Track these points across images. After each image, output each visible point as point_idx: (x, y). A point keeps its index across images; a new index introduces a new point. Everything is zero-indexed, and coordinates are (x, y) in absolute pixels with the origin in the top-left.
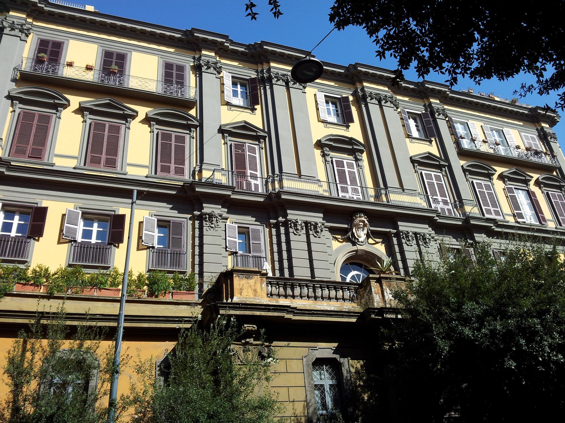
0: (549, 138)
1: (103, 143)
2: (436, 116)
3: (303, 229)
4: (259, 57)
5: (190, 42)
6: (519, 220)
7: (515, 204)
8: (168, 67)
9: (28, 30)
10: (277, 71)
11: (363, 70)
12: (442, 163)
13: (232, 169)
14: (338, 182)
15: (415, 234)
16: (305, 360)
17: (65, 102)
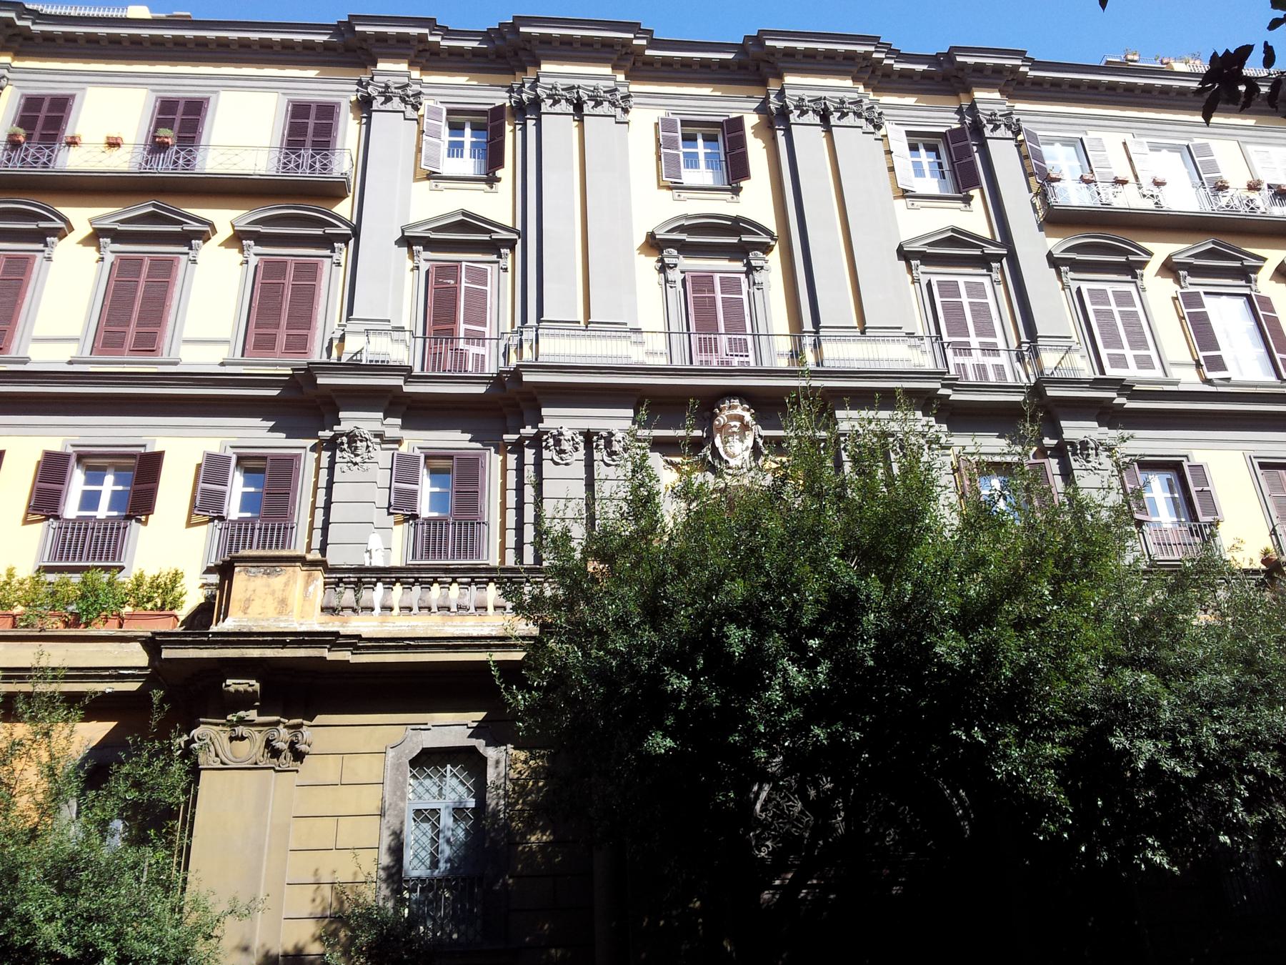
1: (135, 306)
3: (577, 449)
4: (516, 54)
5: (350, 48)
6: (1210, 375)
7: (1202, 332)
9: (418, 94)
10: (593, 83)
11: (780, 44)
13: (688, 329)
14: (693, 329)
16: (391, 753)
17: (59, 224)
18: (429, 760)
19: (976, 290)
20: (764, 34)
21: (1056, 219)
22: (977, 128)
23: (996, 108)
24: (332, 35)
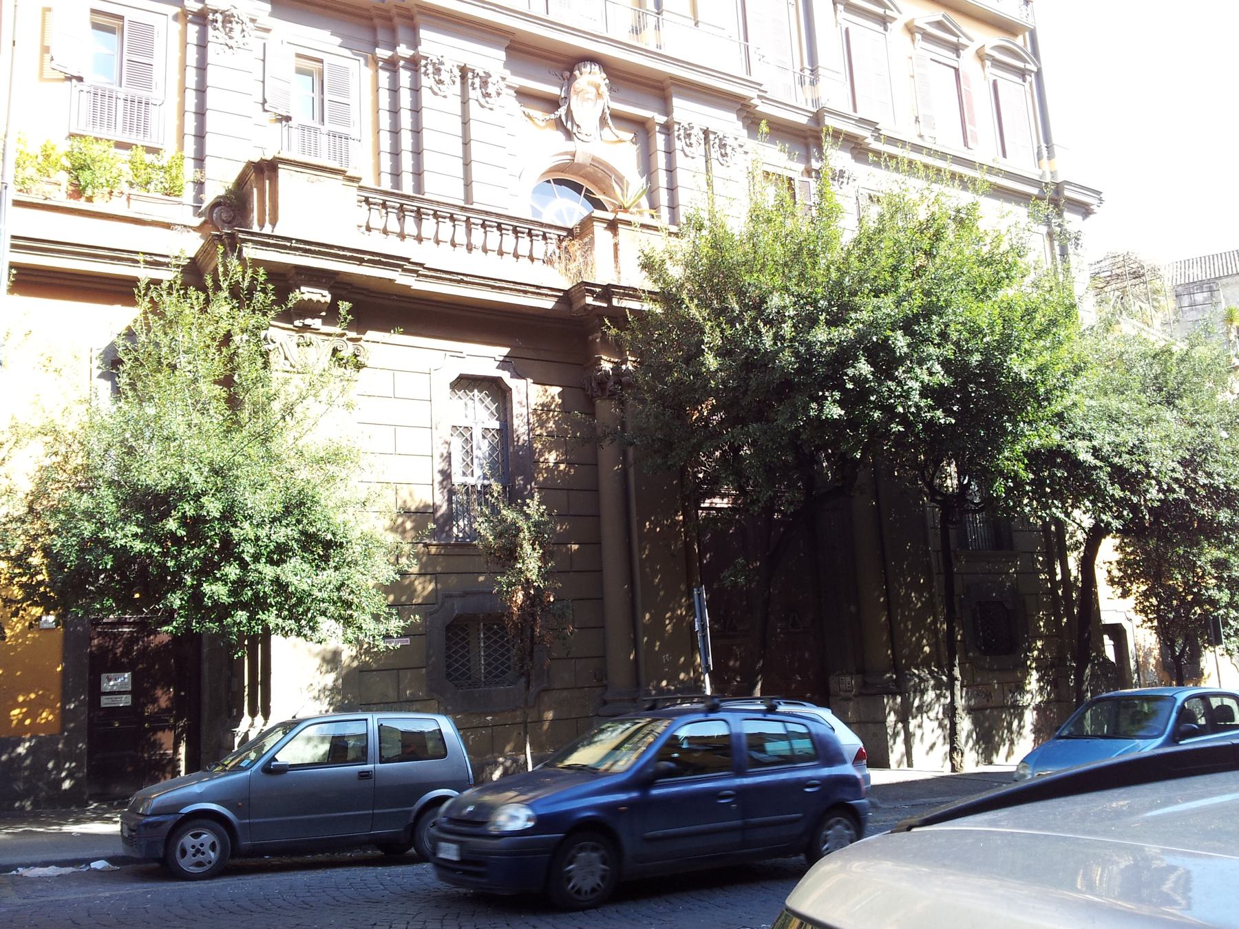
18: (465, 383)
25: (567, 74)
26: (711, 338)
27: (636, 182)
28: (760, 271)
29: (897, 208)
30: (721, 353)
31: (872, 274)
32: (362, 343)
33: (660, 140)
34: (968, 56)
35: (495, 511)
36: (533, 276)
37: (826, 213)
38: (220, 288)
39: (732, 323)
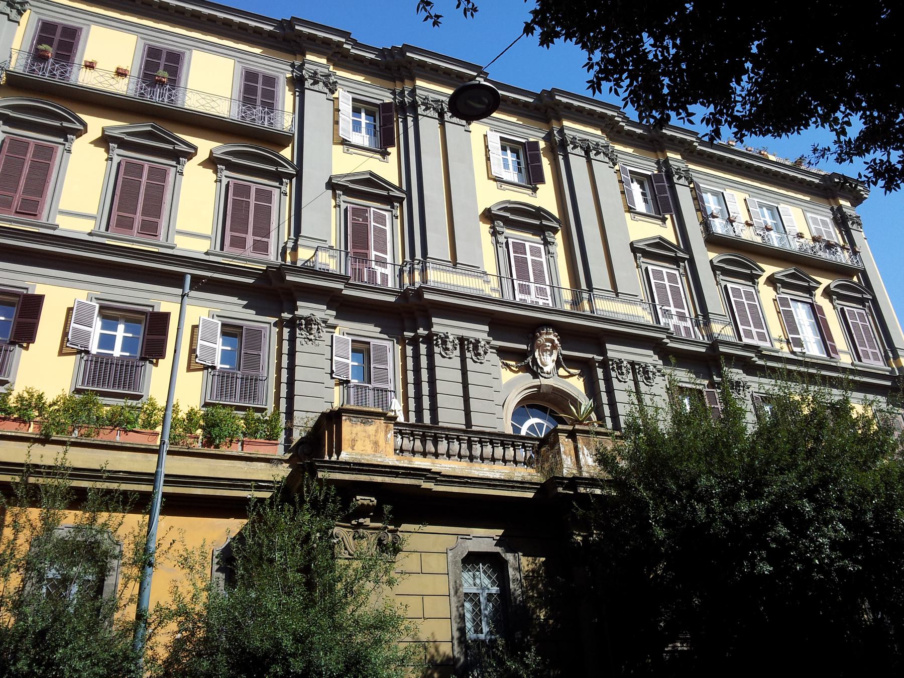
0: (850, 223)
1: (137, 198)
2: (675, 181)
3: (456, 349)
4: (399, 69)
5: (287, 39)
6: (796, 349)
8: (250, 77)
10: (426, 93)
12: (680, 254)
13: (346, 248)
14: (515, 276)
15: (632, 364)
16: (450, 554)
17: (78, 126)
19: (672, 278)
20: (555, 91)
21: (713, 241)
22: (669, 176)
23: (681, 165)
24: (276, 28)
25: (531, 335)
26: (655, 515)
27: (586, 403)
28: (688, 460)
29: (784, 406)
30: (665, 524)
31: (775, 458)
32: (398, 533)
33: (600, 372)
34: (819, 292)
35: (501, 663)
36: (506, 472)
37: (733, 415)
38: (305, 502)
39: (672, 499)
